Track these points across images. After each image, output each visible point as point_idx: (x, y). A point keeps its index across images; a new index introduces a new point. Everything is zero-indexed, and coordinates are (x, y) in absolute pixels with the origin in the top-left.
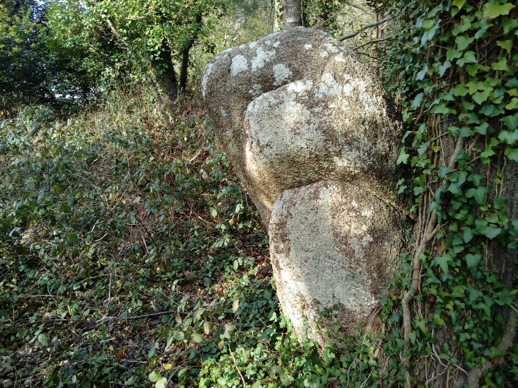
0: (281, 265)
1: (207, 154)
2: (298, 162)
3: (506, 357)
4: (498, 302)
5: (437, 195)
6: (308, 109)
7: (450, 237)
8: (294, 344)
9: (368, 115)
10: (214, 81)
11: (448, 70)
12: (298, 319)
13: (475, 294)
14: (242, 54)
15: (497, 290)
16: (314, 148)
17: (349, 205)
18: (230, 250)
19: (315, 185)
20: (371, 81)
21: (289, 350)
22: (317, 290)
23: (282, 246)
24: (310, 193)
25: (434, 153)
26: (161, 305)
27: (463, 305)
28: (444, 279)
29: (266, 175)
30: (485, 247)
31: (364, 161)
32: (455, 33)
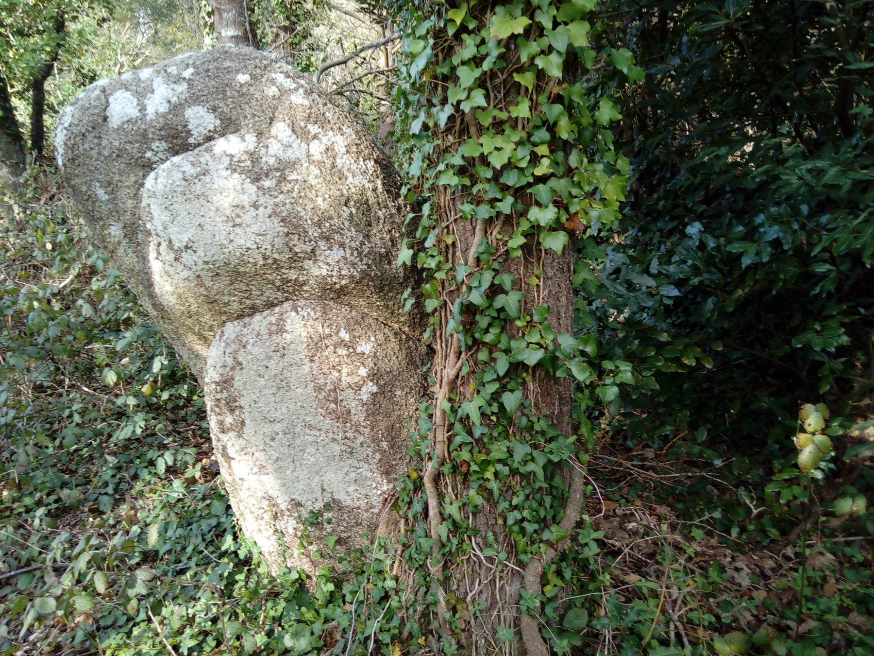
0: (231, 452)
1: (93, 271)
2: (245, 273)
3: (574, 539)
4: (552, 457)
5: (455, 308)
6: (252, 182)
7: (480, 371)
8: (266, 581)
9: (353, 190)
10: (76, 137)
11: (451, 118)
12: (268, 538)
13: (521, 450)
14: (127, 89)
15: (550, 440)
16: (269, 247)
17: (335, 338)
18: (149, 440)
19: (277, 309)
20: (354, 136)
21: (255, 592)
22: (296, 484)
23: (229, 420)
24: (271, 324)
25: (447, 247)
26: (16, 559)
27: (506, 471)
28: (477, 433)
29: (191, 300)
30: (529, 379)
31: (353, 265)
32: (456, 61)
